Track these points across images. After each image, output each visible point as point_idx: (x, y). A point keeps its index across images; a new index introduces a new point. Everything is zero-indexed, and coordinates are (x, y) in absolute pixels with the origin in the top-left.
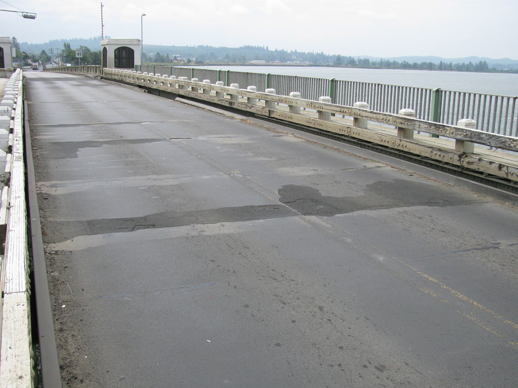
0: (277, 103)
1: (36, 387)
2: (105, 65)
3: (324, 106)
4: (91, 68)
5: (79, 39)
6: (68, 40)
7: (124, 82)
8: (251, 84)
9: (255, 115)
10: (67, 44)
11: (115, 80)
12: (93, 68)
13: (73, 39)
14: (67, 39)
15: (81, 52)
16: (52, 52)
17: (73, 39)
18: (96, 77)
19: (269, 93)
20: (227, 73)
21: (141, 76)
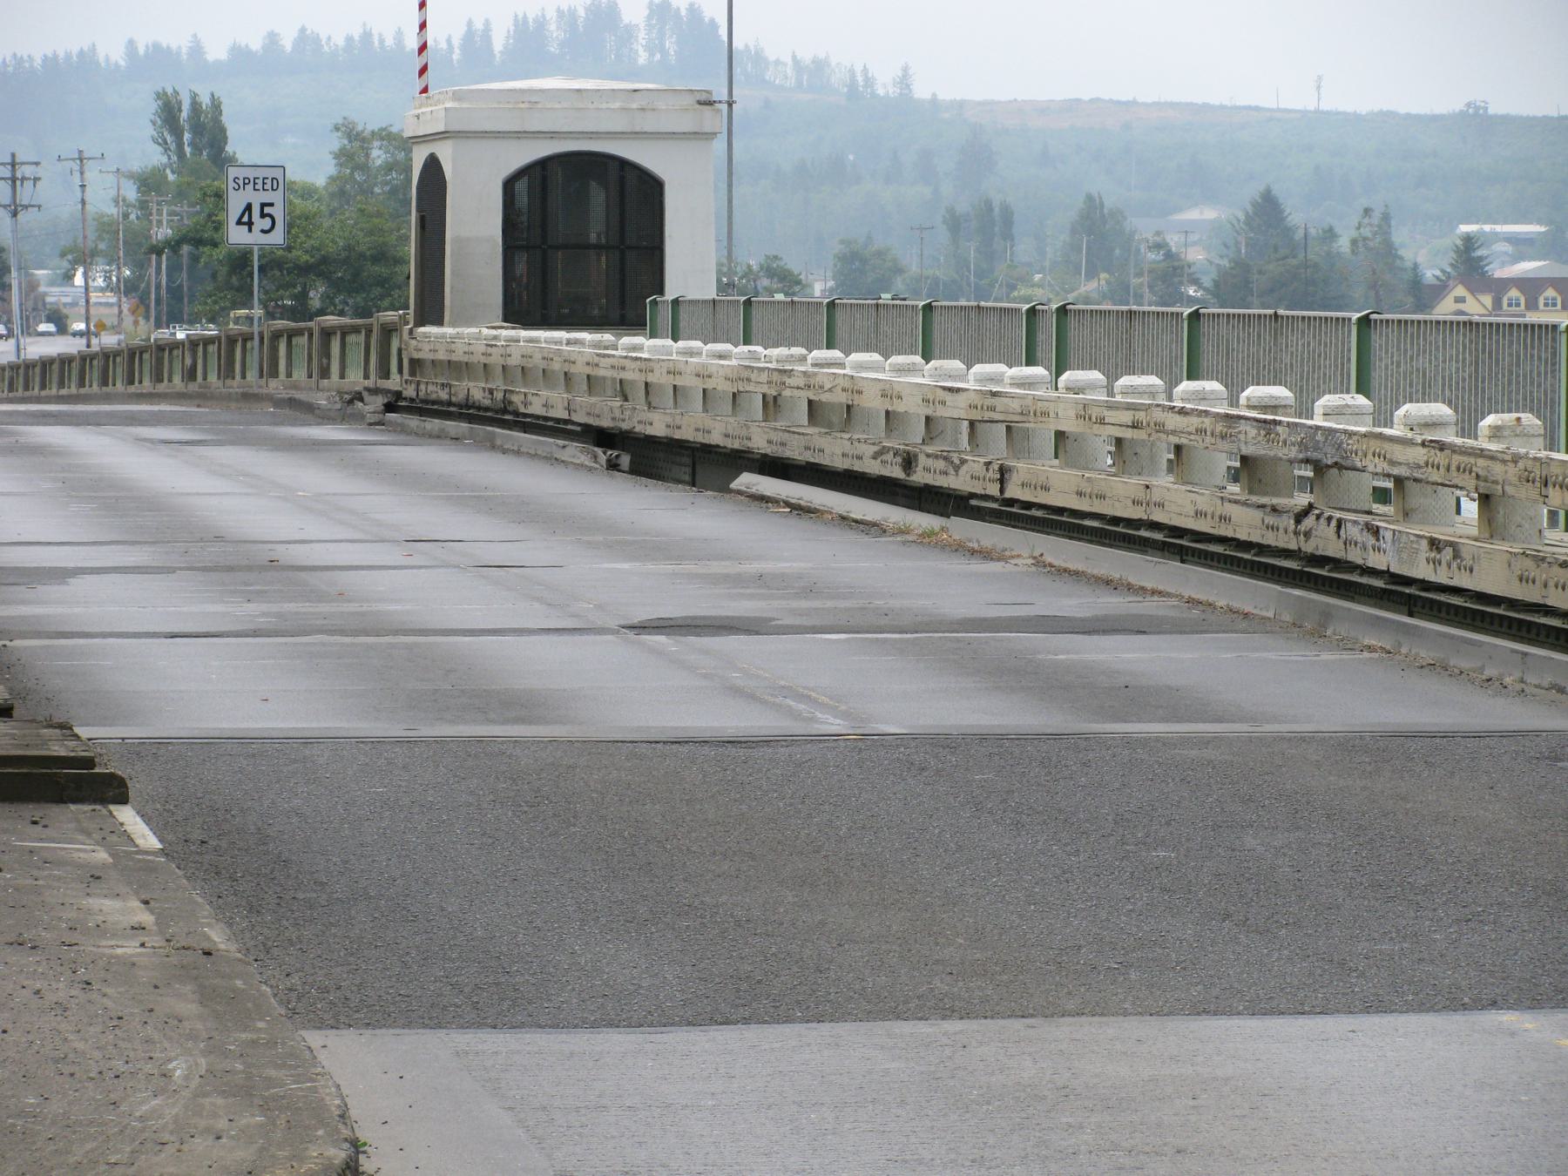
0: (1007, 426)
1: (3, 369)
2: (431, 311)
3: (1106, 413)
4: (351, 339)
5: (340, 41)
6: (210, 57)
7: (516, 413)
8: (1083, 363)
9: (973, 502)
10: (186, 107)
11: (469, 412)
12: (362, 337)
13: (272, 38)
14: (197, 50)
15: (276, 197)
16: (25, 194)
17: (272, 38)
18: (351, 402)
19: (1020, 385)
20: (1055, 315)
21: (596, 359)
